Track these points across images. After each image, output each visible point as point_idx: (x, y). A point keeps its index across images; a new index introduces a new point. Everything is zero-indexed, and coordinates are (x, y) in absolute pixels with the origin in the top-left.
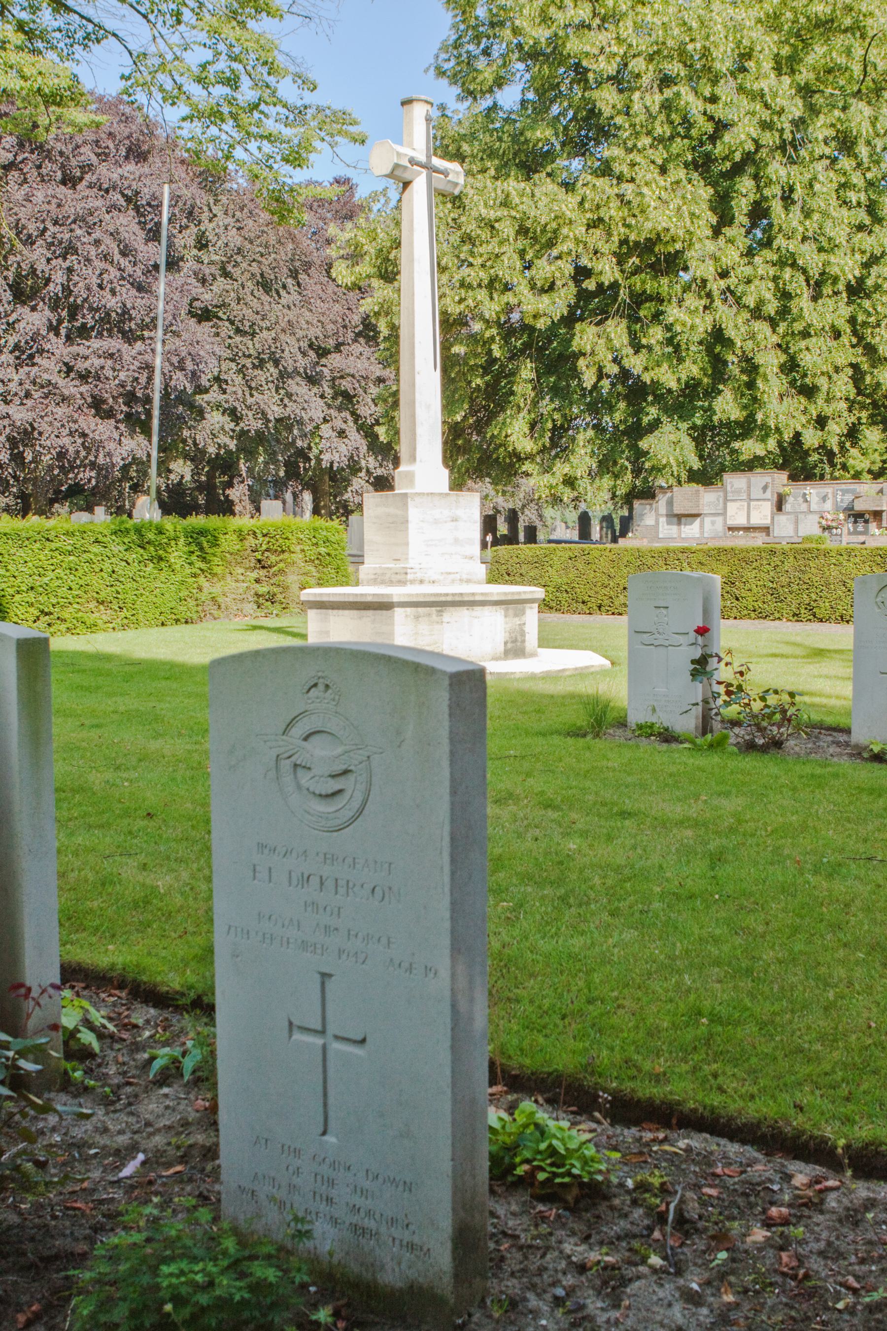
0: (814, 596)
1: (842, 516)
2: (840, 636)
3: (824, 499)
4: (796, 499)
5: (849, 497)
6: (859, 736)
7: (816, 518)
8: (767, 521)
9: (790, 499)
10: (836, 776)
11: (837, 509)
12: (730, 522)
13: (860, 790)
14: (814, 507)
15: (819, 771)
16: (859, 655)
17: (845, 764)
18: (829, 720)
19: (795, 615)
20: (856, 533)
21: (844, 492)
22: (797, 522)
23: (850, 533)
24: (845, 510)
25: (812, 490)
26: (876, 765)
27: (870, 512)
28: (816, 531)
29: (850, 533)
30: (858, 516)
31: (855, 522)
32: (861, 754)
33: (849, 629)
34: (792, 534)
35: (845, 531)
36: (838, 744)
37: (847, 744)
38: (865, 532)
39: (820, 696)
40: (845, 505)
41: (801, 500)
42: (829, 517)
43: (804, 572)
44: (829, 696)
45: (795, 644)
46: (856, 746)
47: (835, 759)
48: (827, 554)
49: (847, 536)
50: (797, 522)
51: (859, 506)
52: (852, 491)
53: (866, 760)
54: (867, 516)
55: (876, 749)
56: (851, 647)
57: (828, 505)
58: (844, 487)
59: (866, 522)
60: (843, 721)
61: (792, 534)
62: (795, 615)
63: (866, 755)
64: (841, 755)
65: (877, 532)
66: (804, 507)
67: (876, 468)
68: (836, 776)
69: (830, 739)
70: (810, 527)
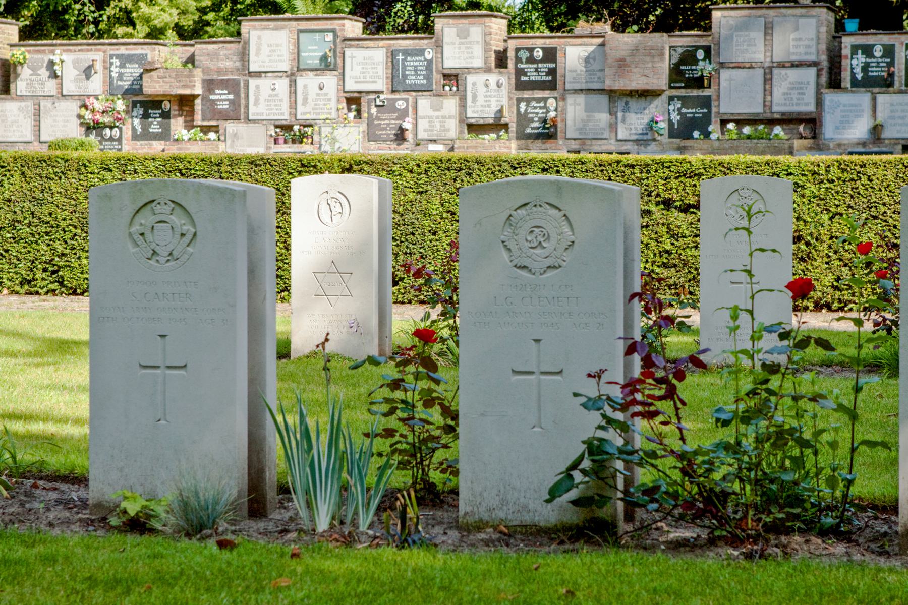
0: (60, 248)
1: (120, 105)
2: (70, 317)
3: (88, 72)
4: (34, 70)
5: (132, 70)
6: (101, 488)
7: (73, 107)
8: (808, 107)
9: (25, 72)
10: (50, 560)
11: (112, 90)
12: (474, 114)
13: (92, 582)
14: (69, 87)
15: (20, 552)
16: (97, 348)
17: (73, 539)
18: (56, 462)
19: (24, 282)
20: (146, 135)
21: (125, 60)
22: (37, 115)
23: (135, 137)
24: (127, 93)
25: (69, 57)
26: (131, 539)
27: (171, 98)
28: (75, 132)
29: (135, 137)
30: (150, 106)
31: (146, 116)
32: (101, 518)
33: (82, 304)
34: (29, 136)
35: (127, 132)
36: (67, 504)
37: (84, 503)
38: (165, 135)
39: (46, 419)
40: (126, 85)
41: (44, 73)
42: (99, 106)
43: (40, 202)
44: (64, 420)
45: (16, 335)
46: (99, 505)
47: (57, 531)
48: (82, 166)
49: (130, 141)
50: (37, 115)
51: (153, 87)
52: (140, 59)
53: (119, 529)
54: (166, 106)
55: (133, 508)
56: (85, 336)
57: (96, 85)
58: (123, 50)
59: (166, 116)
60: (78, 462)
61: (29, 136)
62: (24, 282)
63: (114, 521)
64: (68, 522)
65: (185, 134)
66: (51, 86)
67: (188, 22)
68: (50, 560)
69: (54, 495)
70: (62, 124)
